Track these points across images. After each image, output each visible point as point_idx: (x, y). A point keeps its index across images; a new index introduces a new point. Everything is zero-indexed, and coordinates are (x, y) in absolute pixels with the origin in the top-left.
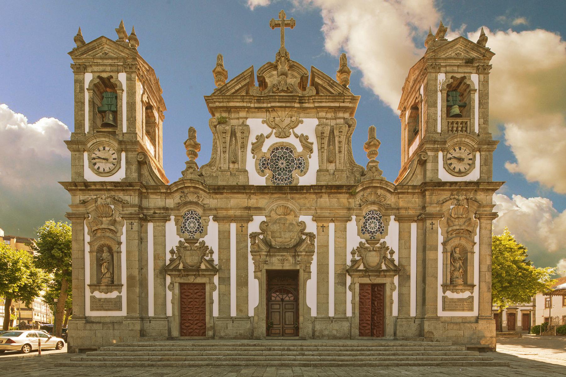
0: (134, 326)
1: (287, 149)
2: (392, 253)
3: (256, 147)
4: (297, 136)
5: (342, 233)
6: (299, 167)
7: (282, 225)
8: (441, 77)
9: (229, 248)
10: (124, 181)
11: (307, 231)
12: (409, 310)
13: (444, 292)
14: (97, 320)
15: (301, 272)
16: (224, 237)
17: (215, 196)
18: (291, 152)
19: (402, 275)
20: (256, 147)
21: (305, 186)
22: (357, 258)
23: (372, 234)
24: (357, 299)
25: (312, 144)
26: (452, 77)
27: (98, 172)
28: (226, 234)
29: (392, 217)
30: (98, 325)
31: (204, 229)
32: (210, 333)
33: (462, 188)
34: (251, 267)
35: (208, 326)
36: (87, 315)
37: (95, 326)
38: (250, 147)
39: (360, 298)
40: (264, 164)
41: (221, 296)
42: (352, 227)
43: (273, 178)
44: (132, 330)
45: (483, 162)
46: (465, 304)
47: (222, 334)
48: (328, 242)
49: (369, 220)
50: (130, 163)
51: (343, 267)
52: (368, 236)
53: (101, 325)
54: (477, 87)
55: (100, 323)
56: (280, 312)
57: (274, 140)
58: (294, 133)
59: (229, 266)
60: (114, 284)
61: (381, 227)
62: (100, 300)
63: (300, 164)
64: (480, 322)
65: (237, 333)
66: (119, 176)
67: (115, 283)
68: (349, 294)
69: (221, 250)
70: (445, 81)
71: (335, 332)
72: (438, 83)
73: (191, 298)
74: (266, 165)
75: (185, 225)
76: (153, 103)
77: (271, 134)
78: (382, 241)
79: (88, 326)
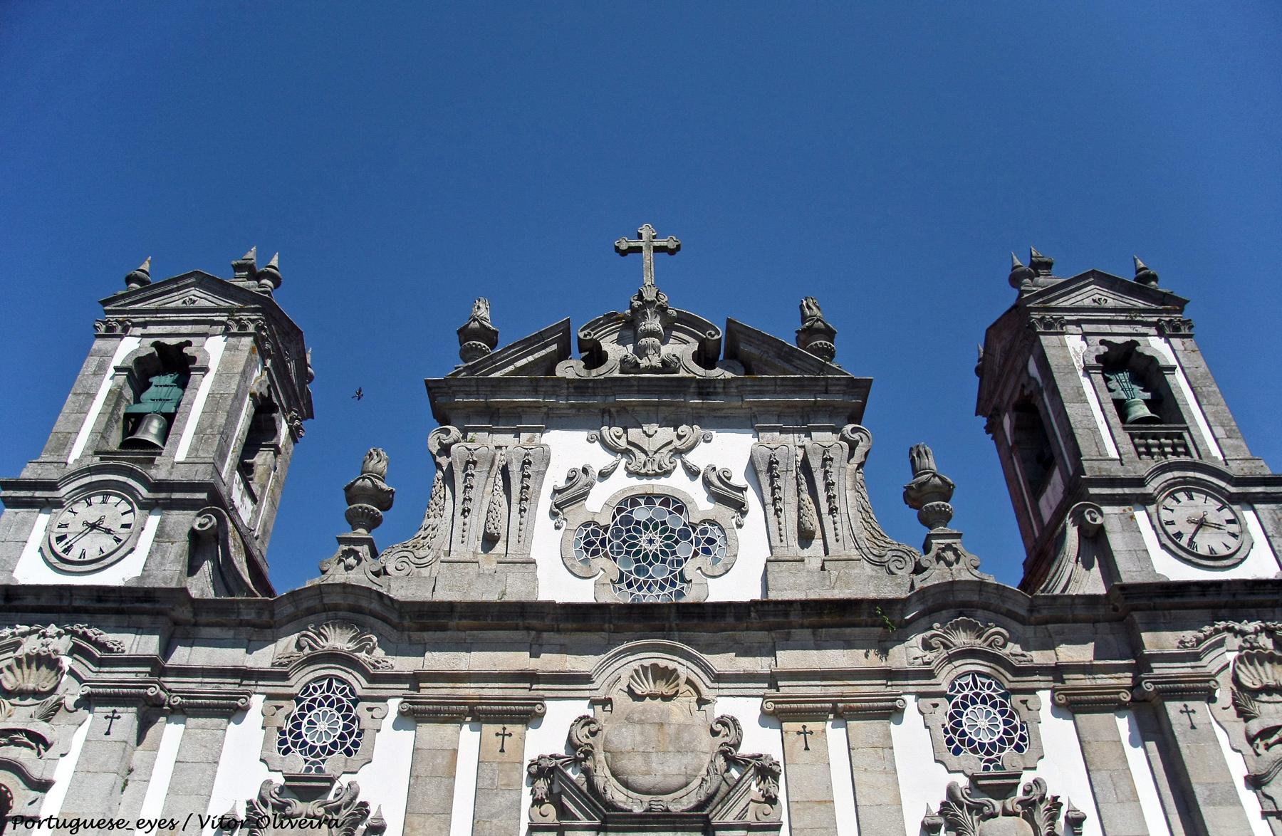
4: (692, 473)
7: (652, 731)
8: (1074, 343)
9: (447, 810)
10: (134, 585)
11: (745, 750)
16: (430, 778)
20: (570, 496)
21: (730, 604)
25: (742, 490)
26: (155, 345)
28: (441, 761)
29: (1045, 697)
33: (1240, 598)
38: (545, 502)
40: (590, 543)
42: (913, 736)
43: (621, 581)
48: (829, 788)
50: (169, 536)
52: (973, 763)
57: (621, 483)
58: (684, 464)
72: (1072, 353)
75: (299, 726)
76: (280, 399)
77: (615, 467)
78: (1027, 778)
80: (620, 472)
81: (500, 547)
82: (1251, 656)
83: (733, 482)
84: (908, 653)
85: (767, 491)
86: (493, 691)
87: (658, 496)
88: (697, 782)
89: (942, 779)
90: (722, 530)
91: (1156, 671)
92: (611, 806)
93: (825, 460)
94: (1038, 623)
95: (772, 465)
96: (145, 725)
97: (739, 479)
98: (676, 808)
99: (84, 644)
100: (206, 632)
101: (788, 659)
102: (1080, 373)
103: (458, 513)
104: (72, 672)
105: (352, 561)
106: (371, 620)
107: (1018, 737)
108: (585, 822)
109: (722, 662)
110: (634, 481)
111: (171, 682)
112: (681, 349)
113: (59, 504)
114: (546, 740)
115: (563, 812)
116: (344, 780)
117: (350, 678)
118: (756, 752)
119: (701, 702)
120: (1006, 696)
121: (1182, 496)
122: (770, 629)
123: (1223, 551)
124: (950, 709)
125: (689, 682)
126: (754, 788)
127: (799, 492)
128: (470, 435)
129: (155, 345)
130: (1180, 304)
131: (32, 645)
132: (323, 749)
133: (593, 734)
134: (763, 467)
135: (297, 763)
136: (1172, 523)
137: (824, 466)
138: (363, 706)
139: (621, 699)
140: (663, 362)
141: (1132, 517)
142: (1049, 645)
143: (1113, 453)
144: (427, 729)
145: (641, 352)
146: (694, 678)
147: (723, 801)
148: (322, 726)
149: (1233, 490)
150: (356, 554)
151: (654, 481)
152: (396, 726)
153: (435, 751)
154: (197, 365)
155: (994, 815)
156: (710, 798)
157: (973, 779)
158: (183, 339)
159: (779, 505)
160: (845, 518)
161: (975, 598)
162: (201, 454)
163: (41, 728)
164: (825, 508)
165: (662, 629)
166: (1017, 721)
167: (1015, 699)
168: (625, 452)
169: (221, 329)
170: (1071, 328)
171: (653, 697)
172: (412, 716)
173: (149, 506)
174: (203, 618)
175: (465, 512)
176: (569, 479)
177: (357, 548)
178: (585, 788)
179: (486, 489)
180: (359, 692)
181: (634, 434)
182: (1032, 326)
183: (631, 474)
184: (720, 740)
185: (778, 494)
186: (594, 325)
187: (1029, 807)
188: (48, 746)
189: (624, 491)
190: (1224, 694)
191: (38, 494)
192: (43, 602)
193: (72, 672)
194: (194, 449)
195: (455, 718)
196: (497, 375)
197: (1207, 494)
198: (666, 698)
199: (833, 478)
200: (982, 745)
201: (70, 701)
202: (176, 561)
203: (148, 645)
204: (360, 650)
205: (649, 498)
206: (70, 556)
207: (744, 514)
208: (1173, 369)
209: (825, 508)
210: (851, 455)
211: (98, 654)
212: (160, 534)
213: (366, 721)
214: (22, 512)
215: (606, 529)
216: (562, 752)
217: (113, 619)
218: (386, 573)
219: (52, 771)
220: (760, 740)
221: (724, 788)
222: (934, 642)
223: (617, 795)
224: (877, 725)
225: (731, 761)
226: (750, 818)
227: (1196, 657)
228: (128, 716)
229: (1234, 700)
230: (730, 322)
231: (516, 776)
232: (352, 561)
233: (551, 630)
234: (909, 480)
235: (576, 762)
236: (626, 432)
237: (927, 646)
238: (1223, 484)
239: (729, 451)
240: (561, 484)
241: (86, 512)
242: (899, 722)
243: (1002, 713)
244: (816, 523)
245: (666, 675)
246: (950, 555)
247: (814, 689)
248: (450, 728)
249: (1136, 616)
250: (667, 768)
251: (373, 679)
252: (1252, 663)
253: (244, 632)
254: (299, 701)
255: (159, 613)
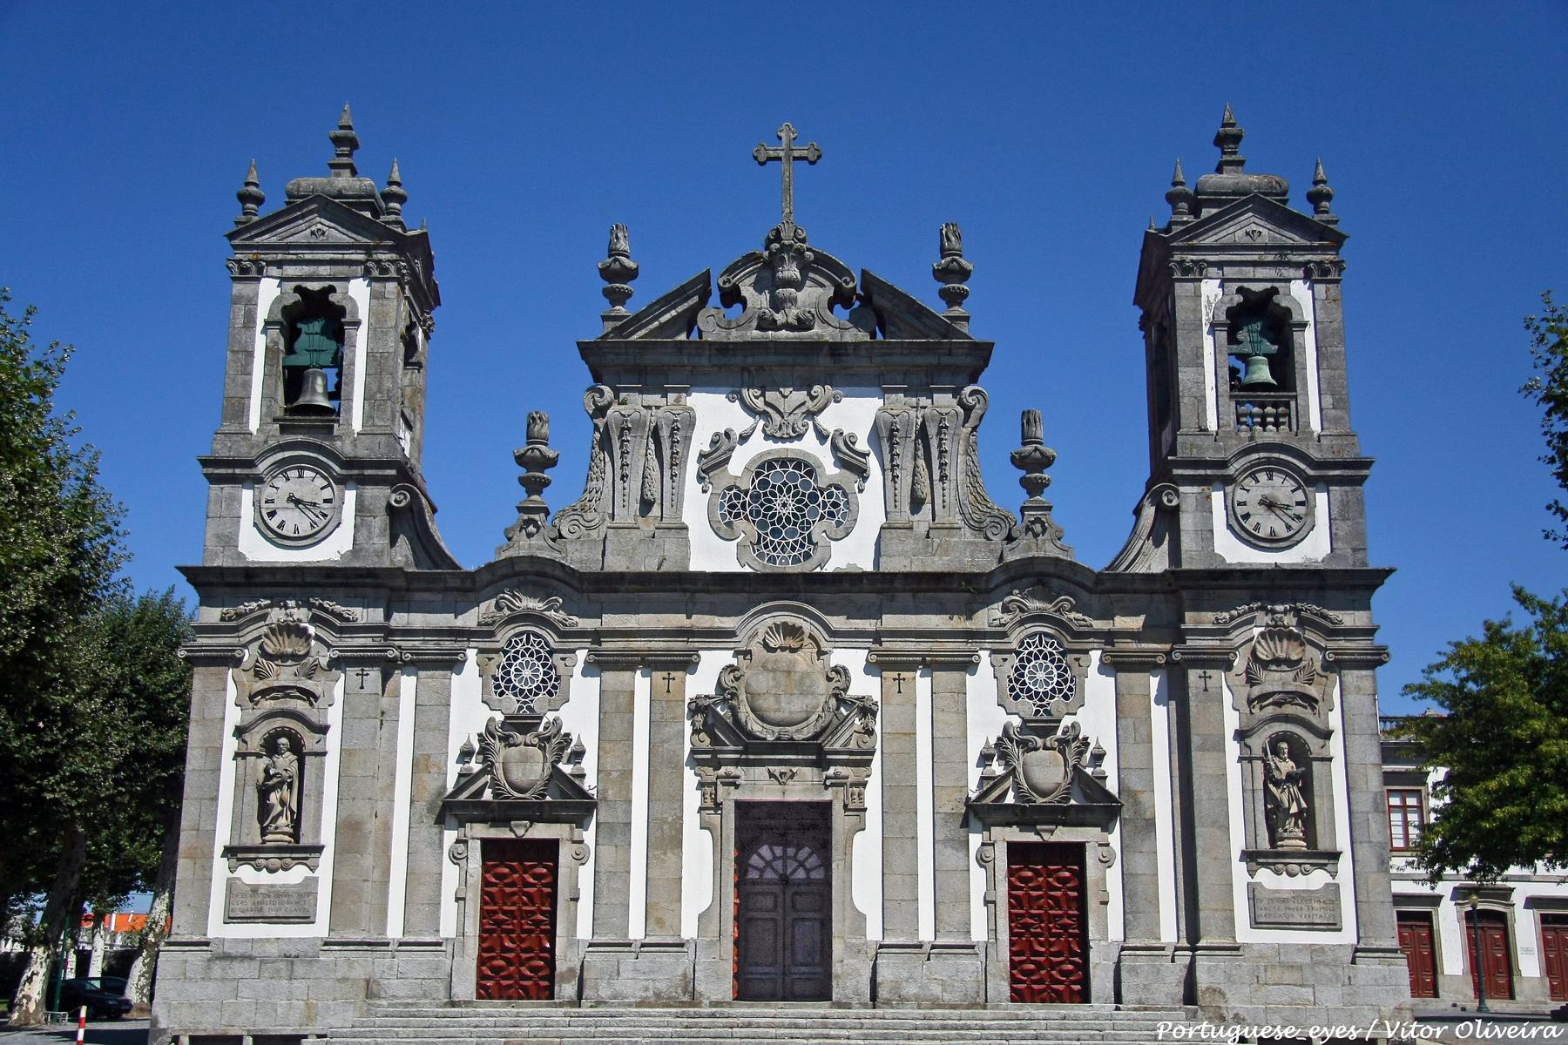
0: (351, 967)
1: (798, 467)
2: (1098, 758)
3: (713, 463)
4: (822, 436)
5: (953, 708)
6: (831, 515)
7: (781, 677)
8: (1210, 289)
9: (629, 738)
11: (853, 691)
12: (1158, 924)
13: (1252, 873)
14: (241, 950)
15: (837, 809)
16: (615, 712)
17: (594, 596)
18: (810, 473)
19: (1130, 820)
20: (713, 463)
22: (997, 769)
23: (1041, 700)
24: (1003, 888)
25: (865, 455)
27: (277, 538)
28: (623, 700)
29: (1095, 655)
30: (246, 964)
31: (562, 684)
32: (567, 990)
34: (692, 798)
35: (560, 967)
36: (211, 934)
37: (239, 969)
38: (692, 467)
39: (1012, 887)
40: (733, 506)
41: (603, 877)
42: (983, 685)
43: (759, 542)
44: (345, 979)
45: (1335, 511)
46: (1316, 905)
47: (604, 993)
49: (1029, 661)
51: (957, 796)
53: (256, 964)
54: (1308, 317)
55: (251, 958)
56: (774, 920)
57: (758, 446)
58: (815, 426)
59: (629, 791)
60: (301, 850)
61: (1066, 681)
62: (255, 889)
63: (835, 505)
64: (1362, 965)
65: (647, 989)
66: (332, 550)
67: (304, 841)
68: (978, 876)
69: (607, 746)
70: (1221, 301)
71: (936, 990)
73: (512, 884)
74: (739, 509)
75: (508, 673)
79: (217, 969)
80: (758, 435)
81: (656, 511)
82: (1275, 633)
83: (858, 447)
84: (989, 616)
85: (887, 457)
86: (658, 644)
87: (792, 460)
88: (814, 717)
89: (1002, 718)
90: (845, 494)
91: (1189, 643)
92: (751, 735)
93: (941, 428)
94: (1102, 592)
95: (892, 433)
96: (386, 677)
97: (862, 445)
98: (798, 737)
99: (324, 615)
100: (418, 596)
101: (891, 621)
102: (1206, 329)
103: (618, 479)
104: (318, 638)
105: (531, 529)
106: (555, 583)
107: (1069, 689)
108: (732, 748)
109: (838, 622)
110: (771, 445)
111: (398, 641)
112: (812, 296)
113: (258, 480)
114: (701, 683)
115: (715, 740)
116: (550, 716)
117: (544, 633)
118: (860, 694)
119: (821, 653)
120: (1063, 654)
121: (1263, 477)
122: (878, 592)
123: (1283, 533)
124: (1016, 662)
125: (811, 637)
126: (857, 721)
127: (915, 457)
128: (622, 395)
129: (298, 289)
130: (1338, 240)
131: (276, 615)
132: (530, 691)
133: (737, 679)
134: (885, 434)
135: (512, 703)
136: (1244, 504)
137: (939, 433)
138: (557, 656)
139: (756, 648)
140: (799, 319)
141: (1209, 497)
142: (1108, 615)
143: (1212, 425)
144: (609, 676)
145: (777, 304)
146: (816, 634)
147: (833, 734)
148: (527, 673)
149: (1311, 472)
150: (534, 522)
151: (788, 445)
152: (584, 674)
153: (618, 693)
154: (348, 318)
155: (1036, 749)
156: (824, 730)
157: (1025, 721)
158: (326, 284)
159: (897, 472)
160: (953, 485)
161: (1052, 570)
162: (377, 422)
163: (308, 684)
164: (936, 476)
165: (791, 591)
166: (1068, 676)
167: (1070, 657)
168: (764, 415)
169: (360, 269)
170: (1213, 271)
171: (783, 649)
172: (597, 665)
173: (342, 481)
174: (415, 585)
175: (623, 477)
176: (713, 443)
177: (536, 517)
178: (730, 721)
179: (640, 450)
180: (553, 645)
181: (771, 396)
182: (1171, 271)
183: (767, 437)
184: (833, 684)
185: (898, 461)
186: (731, 270)
187: (1064, 743)
188: (316, 698)
189: (761, 455)
190: (1240, 663)
191: (238, 471)
192: (279, 578)
193: (318, 638)
194: (367, 418)
195: (631, 667)
196: (634, 338)
197: (1287, 475)
198: (793, 650)
199: (947, 446)
200: (1037, 693)
201: (324, 662)
202: (381, 535)
203: (376, 615)
204: (548, 609)
205: (783, 463)
206: (284, 532)
207: (865, 479)
208: (1304, 325)
209: (936, 476)
210: (966, 421)
211: (338, 623)
212: (361, 509)
213: (561, 670)
214: (227, 488)
215: (746, 493)
216: (713, 693)
217: (341, 592)
218: (561, 536)
219: (326, 717)
220: (864, 686)
221: (835, 722)
222: (1012, 606)
223: (755, 726)
224: (956, 675)
225: (841, 702)
226: (852, 746)
227: (1226, 632)
228: (374, 675)
229: (1248, 668)
230: (864, 273)
231: (679, 711)
232: (531, 529)
233: (702, 591)
234: (1016, 446)
235: (724, 700)
236: (763, 395)
237: (1005, 610)
238: (1303, 466)
239: (854, 414)
240: (707, 449)
241: (284, 486)
242: (973, 674)
243: (1058, 668)
244: (927, 490)
245: (792, 631)
246: (1038, 528)
247: (909, 645)
248: (627, 675)
249: (1184, 594)
250: (792, 706)
251: (563, 635)
252: (1272, 639)
253: (451, 596)
254: (505, 653)
255: (378, 586)
